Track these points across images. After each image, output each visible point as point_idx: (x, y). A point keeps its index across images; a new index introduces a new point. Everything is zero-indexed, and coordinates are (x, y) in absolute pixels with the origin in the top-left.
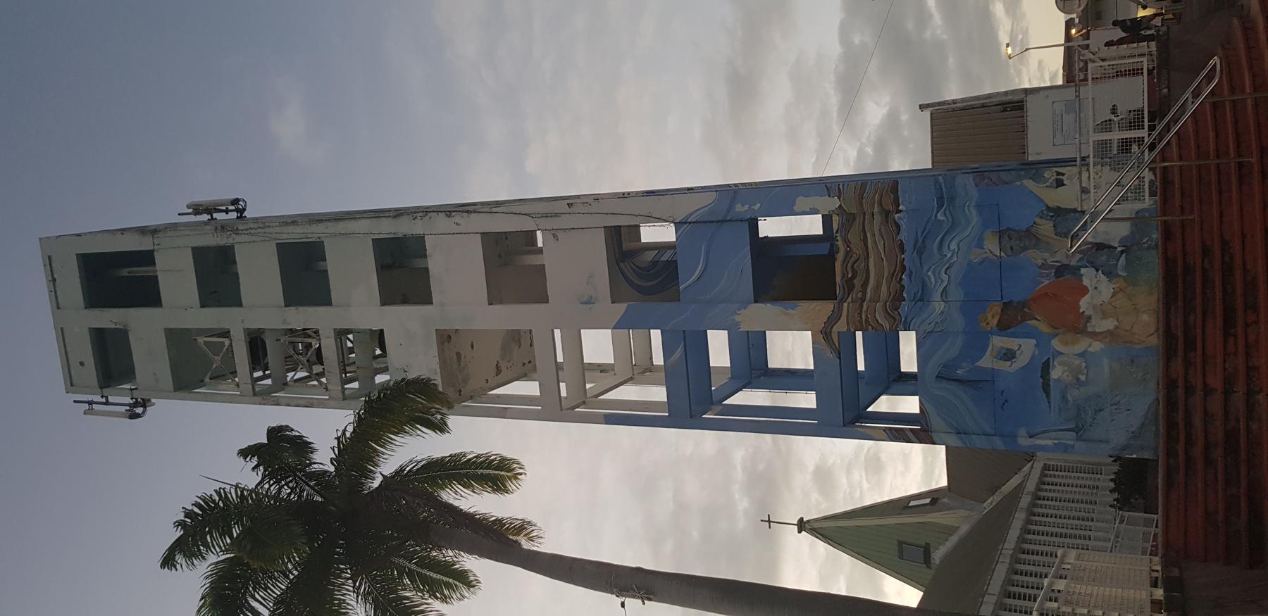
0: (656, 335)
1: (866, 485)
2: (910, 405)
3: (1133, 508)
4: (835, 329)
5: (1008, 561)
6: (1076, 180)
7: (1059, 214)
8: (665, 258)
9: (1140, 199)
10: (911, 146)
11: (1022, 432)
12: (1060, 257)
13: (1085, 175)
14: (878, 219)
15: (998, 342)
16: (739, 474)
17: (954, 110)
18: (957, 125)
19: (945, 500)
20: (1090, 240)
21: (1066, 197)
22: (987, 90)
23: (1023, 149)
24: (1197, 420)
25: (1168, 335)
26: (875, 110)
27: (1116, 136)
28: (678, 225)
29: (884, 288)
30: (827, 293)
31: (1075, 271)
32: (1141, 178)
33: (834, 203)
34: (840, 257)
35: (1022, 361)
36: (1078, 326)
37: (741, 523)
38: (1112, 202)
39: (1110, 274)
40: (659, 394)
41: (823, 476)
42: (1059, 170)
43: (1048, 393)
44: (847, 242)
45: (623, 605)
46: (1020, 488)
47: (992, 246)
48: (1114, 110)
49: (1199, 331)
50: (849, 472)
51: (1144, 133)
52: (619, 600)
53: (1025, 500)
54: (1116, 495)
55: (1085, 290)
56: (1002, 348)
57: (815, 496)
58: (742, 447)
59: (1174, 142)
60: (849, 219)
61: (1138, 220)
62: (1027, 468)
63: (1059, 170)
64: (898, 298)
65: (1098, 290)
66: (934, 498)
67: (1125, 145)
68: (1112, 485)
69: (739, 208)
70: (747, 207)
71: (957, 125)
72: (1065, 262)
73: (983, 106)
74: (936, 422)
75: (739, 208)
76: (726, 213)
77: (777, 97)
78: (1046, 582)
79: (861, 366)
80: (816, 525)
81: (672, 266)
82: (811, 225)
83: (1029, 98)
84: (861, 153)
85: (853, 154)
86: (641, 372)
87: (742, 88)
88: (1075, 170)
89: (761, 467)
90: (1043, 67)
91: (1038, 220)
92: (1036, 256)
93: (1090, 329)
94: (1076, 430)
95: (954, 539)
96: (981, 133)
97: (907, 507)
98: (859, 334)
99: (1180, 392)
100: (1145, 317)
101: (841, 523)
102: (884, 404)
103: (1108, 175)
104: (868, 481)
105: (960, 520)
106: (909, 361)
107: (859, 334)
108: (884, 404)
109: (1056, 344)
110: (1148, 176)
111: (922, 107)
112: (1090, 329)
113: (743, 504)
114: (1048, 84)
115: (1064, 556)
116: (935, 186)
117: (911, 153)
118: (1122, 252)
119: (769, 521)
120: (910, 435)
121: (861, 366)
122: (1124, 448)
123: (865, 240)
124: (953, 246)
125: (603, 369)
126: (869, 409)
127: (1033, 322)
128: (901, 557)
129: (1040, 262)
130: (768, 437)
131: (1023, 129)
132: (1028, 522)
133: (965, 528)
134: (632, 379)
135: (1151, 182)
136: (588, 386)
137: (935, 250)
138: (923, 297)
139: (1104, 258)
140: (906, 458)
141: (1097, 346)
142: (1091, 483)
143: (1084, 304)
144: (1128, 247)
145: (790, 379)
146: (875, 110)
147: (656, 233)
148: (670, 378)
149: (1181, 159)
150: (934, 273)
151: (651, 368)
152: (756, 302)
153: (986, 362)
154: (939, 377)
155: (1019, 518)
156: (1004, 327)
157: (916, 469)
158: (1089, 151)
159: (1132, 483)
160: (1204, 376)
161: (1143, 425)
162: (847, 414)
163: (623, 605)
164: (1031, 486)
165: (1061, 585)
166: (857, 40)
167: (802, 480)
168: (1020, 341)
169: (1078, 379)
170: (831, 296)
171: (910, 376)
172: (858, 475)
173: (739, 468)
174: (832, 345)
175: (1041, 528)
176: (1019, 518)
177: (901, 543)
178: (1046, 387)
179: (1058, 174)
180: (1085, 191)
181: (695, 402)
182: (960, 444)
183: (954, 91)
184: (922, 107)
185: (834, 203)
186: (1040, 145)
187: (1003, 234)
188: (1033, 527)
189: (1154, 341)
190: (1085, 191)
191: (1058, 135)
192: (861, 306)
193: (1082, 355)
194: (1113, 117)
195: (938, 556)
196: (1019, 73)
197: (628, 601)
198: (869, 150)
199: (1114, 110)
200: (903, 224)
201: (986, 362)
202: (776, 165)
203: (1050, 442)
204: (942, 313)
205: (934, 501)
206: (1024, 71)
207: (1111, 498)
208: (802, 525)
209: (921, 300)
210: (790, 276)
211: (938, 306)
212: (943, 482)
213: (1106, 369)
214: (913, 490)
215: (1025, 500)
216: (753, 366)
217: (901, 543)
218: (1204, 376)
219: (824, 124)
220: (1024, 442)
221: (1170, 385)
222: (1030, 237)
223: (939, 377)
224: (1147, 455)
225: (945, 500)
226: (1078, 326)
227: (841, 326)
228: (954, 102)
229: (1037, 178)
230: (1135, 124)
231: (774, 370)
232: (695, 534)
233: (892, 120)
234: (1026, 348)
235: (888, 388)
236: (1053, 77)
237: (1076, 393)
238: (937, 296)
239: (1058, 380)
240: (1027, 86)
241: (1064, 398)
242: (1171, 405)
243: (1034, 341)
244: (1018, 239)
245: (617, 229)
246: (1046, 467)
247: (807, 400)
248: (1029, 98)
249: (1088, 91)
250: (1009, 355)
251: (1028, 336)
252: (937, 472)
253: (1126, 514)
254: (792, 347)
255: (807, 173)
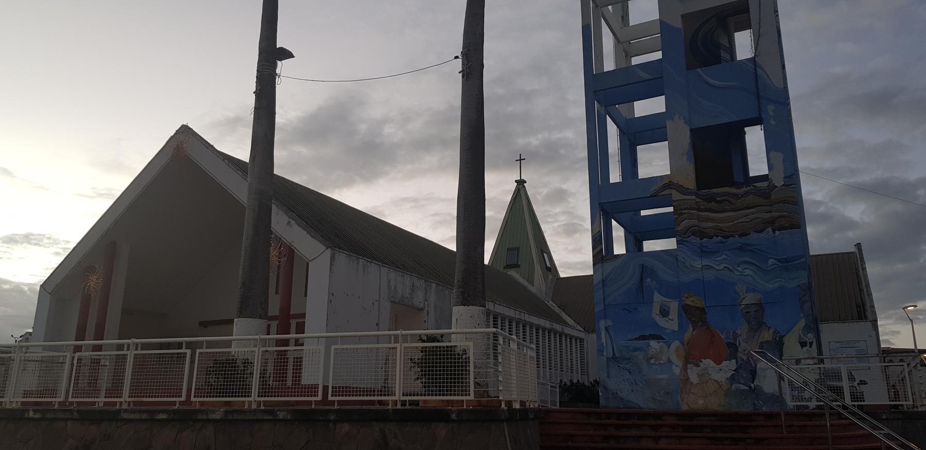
0: (658, 55)
1: (556, 224)
2: (619, 249)
3: (561, 394)
4: (673, 191)
5: (517, 316)
6: (806, 355)
7: (778, 346)
8: (723, 53)
9: (793, 398)
10: (826, 241)
11: (610, 323)
12: (743, 346)
13: (811, 361)
14: (768, 215)
15: (674, 306)
16: (556, 136)
17: (857, 269)
18: (846, 272)
19: (550, 276)
20: (759, 366)
21: (791, 347)
22: (875, 295)
23: (827, 320)
24: (634, 432)
25: (692, 415)
26: (857, 211)
27: (845, 384)
28: (753, 60)
29: (710, 224)
30: (703, 180)
31: (733, 355)
32: (810, 400)
33: (778, 181)
34: (733, 190)
35: (661, 322)
36: (691, 358)
37: (521, 141)
38: (788, 378)
39: (732, 379)
40: (609, 65)
41: (560, 196)
42: (814, 344)
43: (636, 339)
44: (746, 194)
45: (457, 57)
46: (565, 324)
47: (749, 299)
48: (863, 382)
49: (698, 434)
50: (564, 213)
51: (848, 401)
52: (459, 54)
53: (558, 327)
54: (568, 383)
55: (718, 362)
56: (669, 308)
57: (545, 191)
58: (576, 135)
59: (847, 422)
60: (766, 194)
61: (778, 398)
62: (579, 327)
63: (814, 344)
64: (702, 234)
65: (720, 372)
66: (551, 269)
67: (839, 391)
68: (575, 381)
69: (771, 108)
70: (771, 114)
71: (846, 272)
72: (740, 350)
73: (861, 290)
74: (609, 267)
75: (771, 108)
76: (766, 98)
77: (869, 132)
78: (514, 337)
79: (644, 213)
80: (522, 192)
81: (718, 60)
82: (758, 165)
83: (869, 324)
84: (820, 203)
85: (819, 197)
86: (624, 49)
87: (879, 102)
88: (815, 354)
89: (562, 151)
90: (895, 333)
91: (772, 331)
92: (743, 330)
93: (689, 366)
94: (614, 358)
95: (525, 283)
96: (841, 290)
97: (542, 252)
98: (671, 209)
99: (653, 422)
100: (701, 402)
101: (526, 208)
102: (618, 232)
103: (813, 377)
104: (559, 226)
105: (539, 287)
106: (650, 246)
107: (671, 209)
108: (618, 232)
109: (676, 344)
110: (813, 404)
111: (858, 245)
112: (689, 366)
113: (534, 141)
114: (881, 338)
115: (531, 349)
116: (797, 257)
117: (819, 239)
118: (750, 387)
119: (521, 160)
120: (598, 249)
121: (644, 213)
122: (605, 387)
123: (747, 208)
124: (747, 272)
125: (625, 17)
126: (614, 223)
127: (691, 329)
128: (509, 250)
129: (739, 332)
130: (584, 154)
131: (841, 320)
132: (544, 329)
133: (533, 289)
134: (619, 42)
135: (807, 407)
136: (610, 7)
137: (742, 259)
138: (703, 252)
139: (745, 375)
140: (579, 250)
141: (677, 371)
142: (575, 368)
143: (708, 363)
144: (756, 392)
145: (630, 163)
146: (857, 211)
147: (744, 44)
148: (624, 71)
149: (831, 425)
150: (724, 259)
151: (629, 56)
152: (691, 130)
153: (657, 298)
154: (643, 267)
155: (547, 324)
156: (686, 309)
157: (572, 254)
158: (828, 365)
159: (579, 394)
160: (666, 437)
161: (622, 399)
162: (607, 205)
163: (457, 57)
164: (568, 331)
165: (514, 346)
166: (921, 192)
167: (555, 181)
168: (676, 321)
169: (651, 358)
170: (699, 187)
171: (640, 248)
172: (563, 219)
173: (559, 136)
174: (659, 191)
175: (541, 340)
176: (547, 324)
177: (518, 249)
178: (643, 338)
179: (811, 344)
180: (798, 362)
181: (606, 94)
182: (595, 283)
183: (873, 270)
184: (858, 245)
185: (778, 181)
186: (830, 332)
187: (760, 307)
188: (541, 332)
189: (684, 408)
190: (798, 362)
191: (838, 345)
192: (693, 209)
193: (669, 361)
194: (857, 382)
195: (512, 273)
196: (889, 317)
197: (460, 61)
198: (822, 209)
199: (863, 382)
200: (763, 235)
201: (657, 298)
202: (807, 138)
203: (603, 340)
204: (692, 266)
205: (549, 269)
206: (890, 321)
207: (566, 380)
208: (521, 183)
209: (702, 251)
210: (714, 154)
211: (698, 264)
212: (562, 275)
213: (662, 377)
214: (555, 257)
215: (558, 327)
216: (637, 134)
217: (518, 249)
218: (666, 437)
219: (837, 173)
220: (602, 324)
221: (657, 415)
222: (758, 325)
223: (643, 267)
224: (602, 402)
225: (550, 276)
226: (691, 358)
227: (676, 195)
228: (864, 269)
229: (807, 329)
230: (854, 397)
231: (635, 150)
232: (510, 109)
233: (850, 224)
234: (671, 324)
235: (630, 233)
236: (887, 341)
237: (641, 357)
238: (706, 262)
239: (649, 345)
240: (879, 323)
241: (636, 349)
242: (644, 416)
243: (676, 329)
244: (756, 317)
245: (747, 10)
246: (582, 340)
247: (615, 176)
248: (869, 324)
249: (876, 364)
250: (664, 313)
251: (681, 325)
252: (571, 271)
253: (558, 390)
254: (655, 162)
255: (802, 163)
